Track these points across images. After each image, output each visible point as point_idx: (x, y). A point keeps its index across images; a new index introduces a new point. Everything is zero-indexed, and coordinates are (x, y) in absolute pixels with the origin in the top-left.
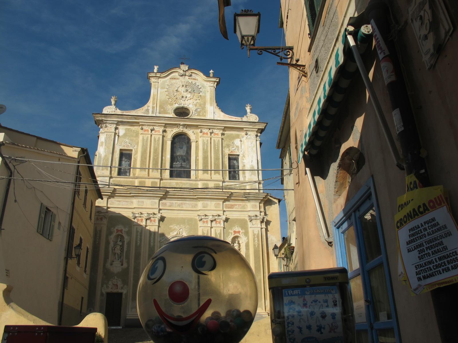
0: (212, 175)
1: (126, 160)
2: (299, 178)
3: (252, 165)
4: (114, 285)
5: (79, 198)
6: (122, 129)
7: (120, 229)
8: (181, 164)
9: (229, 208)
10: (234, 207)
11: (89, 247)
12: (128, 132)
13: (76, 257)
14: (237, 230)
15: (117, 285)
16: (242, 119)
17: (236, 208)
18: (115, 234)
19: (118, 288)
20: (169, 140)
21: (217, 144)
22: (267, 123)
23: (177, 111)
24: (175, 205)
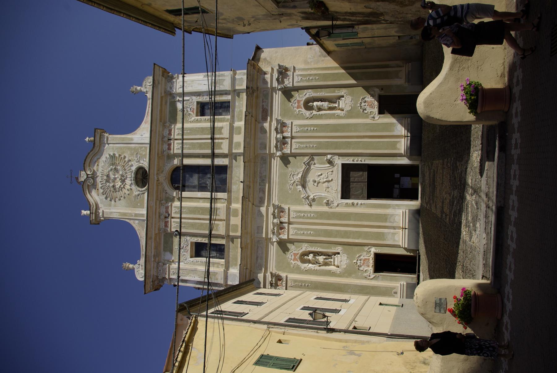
0: (223, 137)
5: (248, 313)
6: (164, 255)
10: (265, 108)
11: (315, 297)
13: (326, 317)
16: (149, 99)
17: (267, 106)
18: (299, 263)
20: (181, 194)
22: (155, 64)
23: (141, 185)
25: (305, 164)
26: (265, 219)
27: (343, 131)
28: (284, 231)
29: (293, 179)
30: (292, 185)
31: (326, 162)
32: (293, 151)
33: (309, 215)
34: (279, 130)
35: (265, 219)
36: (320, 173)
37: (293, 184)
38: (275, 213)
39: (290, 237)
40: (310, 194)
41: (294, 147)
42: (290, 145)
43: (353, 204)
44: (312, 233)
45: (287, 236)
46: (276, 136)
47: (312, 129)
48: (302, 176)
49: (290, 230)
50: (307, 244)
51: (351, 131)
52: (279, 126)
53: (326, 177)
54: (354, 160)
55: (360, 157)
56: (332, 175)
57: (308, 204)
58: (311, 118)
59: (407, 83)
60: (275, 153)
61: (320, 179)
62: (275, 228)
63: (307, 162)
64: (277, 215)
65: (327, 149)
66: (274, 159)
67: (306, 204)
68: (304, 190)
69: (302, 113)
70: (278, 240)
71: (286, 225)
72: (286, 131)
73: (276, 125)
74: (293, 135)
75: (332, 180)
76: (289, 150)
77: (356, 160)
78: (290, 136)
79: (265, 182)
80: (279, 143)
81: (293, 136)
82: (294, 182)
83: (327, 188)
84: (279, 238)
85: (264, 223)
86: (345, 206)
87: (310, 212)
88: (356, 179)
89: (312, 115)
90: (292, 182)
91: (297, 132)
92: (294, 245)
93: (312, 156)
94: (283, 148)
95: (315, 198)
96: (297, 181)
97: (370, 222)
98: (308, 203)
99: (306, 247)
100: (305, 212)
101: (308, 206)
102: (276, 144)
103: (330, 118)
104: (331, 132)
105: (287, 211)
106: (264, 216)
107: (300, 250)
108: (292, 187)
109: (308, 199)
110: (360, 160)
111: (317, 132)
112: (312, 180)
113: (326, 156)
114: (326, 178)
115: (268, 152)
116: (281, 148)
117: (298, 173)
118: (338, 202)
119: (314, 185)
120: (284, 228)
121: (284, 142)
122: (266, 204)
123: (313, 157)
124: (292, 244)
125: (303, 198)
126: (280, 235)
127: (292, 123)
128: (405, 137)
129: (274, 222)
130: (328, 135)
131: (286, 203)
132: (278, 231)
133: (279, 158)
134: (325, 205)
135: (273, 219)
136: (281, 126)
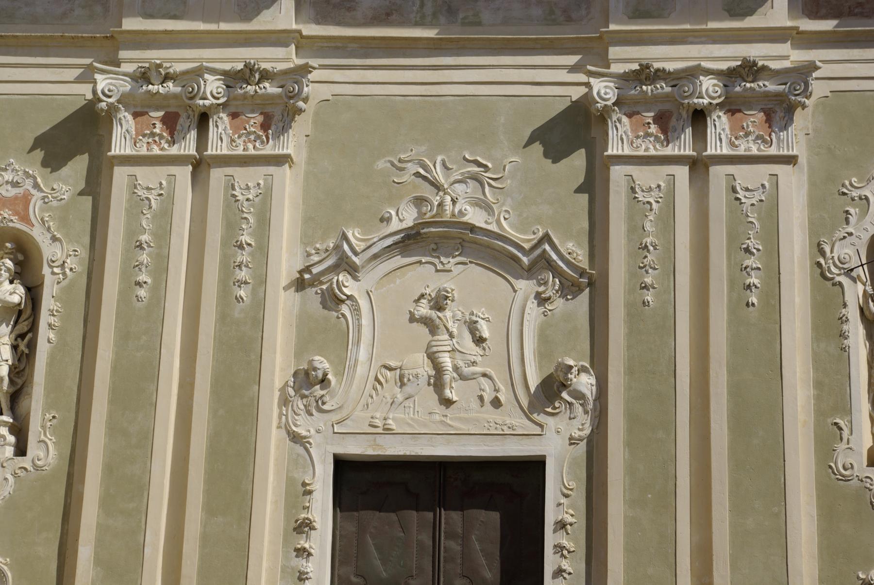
25: (540, 242)
26: (224, 26)
27: (737, 464)
28: (153, 135)
29: (452, 179)
30: (417, 175)
31: (552, 370)
32: (617, 172)
33: (243, 274)
34: (745, 89)
35: (224, 26)
36: (486, 334)
37: (425, 178)
38: (258, 83)
39: (120, 174)
40: (370, 277)
41: (644, 176)
42: (652, 152)
43: (304, 527)
44: (142, 293)
45: (129, 151)
46: (708, 72)
47: (754, 280)
48: (473, 228)
49: (162, 172)
50: (78, 268)
51: (738, 508)
52: (772, 87)
53: (467, 370)
54: (562, 532)
55: (583, 566)
56: (475, 404)
57: (307, 269)
58: (823, 275)
60: (609, 68)
61: (451, 336)
62: (171, 87)
63: (554, 256)
64: (245, 96)
65: (630, 371)
66: (574, 69)
67: (309, 255)
68: (389, 241)
69: (852, 220)
70: (103, 105)
71: (684, 146)
72: (739, 131)
73: (774, 65)
74: (718, 172)
75: (447, 403)
76: (627, 151)
77: (565, 542)
78: (710, 151)
79: (442, 19)
80: (668, 89)
81: (708, 170)
82: (437, 187)
83: (401, 377)
84: (117, 110)
85: (205, 20)
86: (290, 481)
87: (262, 280)
88: (455, 546)
89: (838, 279)
90: (439, 175)
91: (734, 190)
92: (81, 194)
93: (590, 284)
94: (638, 113)
95: (345, 309)
96: (441, 205)
97: (364, 60)
98: (315, 270)
99: (62, 266)
100: (262, 250)
101: (300, 267)
102: (661, 75)
103: (818, 385)
104: (736, 391)
105: (269, 150)
106: (248, 19)
107: (49, 229)
108: (407, 177)
109: (335, 268)
110: (565, 565)
111: (733, 311)
112: (448, 286)
113: (592, 364)
114: (456, 369)
115: (613, 27)
116: (636, 102)
117: (487, 208)
118: (315, 440)
119: (417, 301)
120: (172, 134)
121: (674, 119)
122: (311, 30)
123: (581, 291)
124: (82, 185)
125: (345, 237)
126: (136, 115)
127: (791, 160)
129: (206, 76)
130: (712, 373)
131: (314, 144)
132: (155, 100)
133: (577, 93)
134: (305, 366)
135: (225, 73)
136: (767, 95)
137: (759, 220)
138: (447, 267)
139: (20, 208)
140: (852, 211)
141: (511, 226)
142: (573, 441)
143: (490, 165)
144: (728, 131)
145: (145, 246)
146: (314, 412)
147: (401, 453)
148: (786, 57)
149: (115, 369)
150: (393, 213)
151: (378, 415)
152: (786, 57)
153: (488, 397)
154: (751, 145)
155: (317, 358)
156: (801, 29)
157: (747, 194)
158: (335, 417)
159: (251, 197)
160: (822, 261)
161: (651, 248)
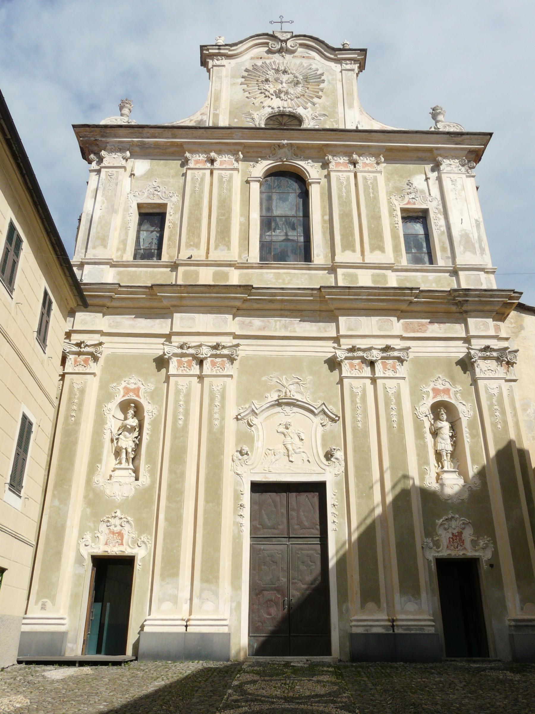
1: (152, 229)
2: (3, 430)
3: (464, 230)
4: (113, 533)
7: (132, 386)
8: (286, 235)
9: (414, 332)
12: (156, 167)
14: (441, 387)
15: (120, 534)
19: (124, 543)
21: (371, 186)
24: (276, 325)
28: (184, 367)
46: (375, 349)
53: (297, 451)
57: (239, 415)
59: (513, 623)
65: (355, 451)
82: (284, 387)
87: (223, 419)
89: (422, 419)
90: (284, 382)
98: (242, 415)
100: (223, 407)
112: (289, 421)
114: (294, 450)
117: (302, 393)
118: (244, 475)
127: (231, 376)
128: (389, 620)
137: (395, 398)
138: (289, 414)
139: (136, 392)
140: (424, 396)
141: (310, 400)
142: (336, 475)
143: (302, 379)
144: (382, 369)
145: (181, 405)
146: (243, 465)
147: (275, 480)
148: (399, 345)
149: (171, 449)
150: (269, 395)
151: (266, 466)
152: (399, 345)
153: (306, 459)
154: (390, 373)
155: (244, 446)
156: (403, 336)
157: (390, 389)
158: (251, 467)
159: (219, 389)
160: (416, 413)
161: (359, 408)
